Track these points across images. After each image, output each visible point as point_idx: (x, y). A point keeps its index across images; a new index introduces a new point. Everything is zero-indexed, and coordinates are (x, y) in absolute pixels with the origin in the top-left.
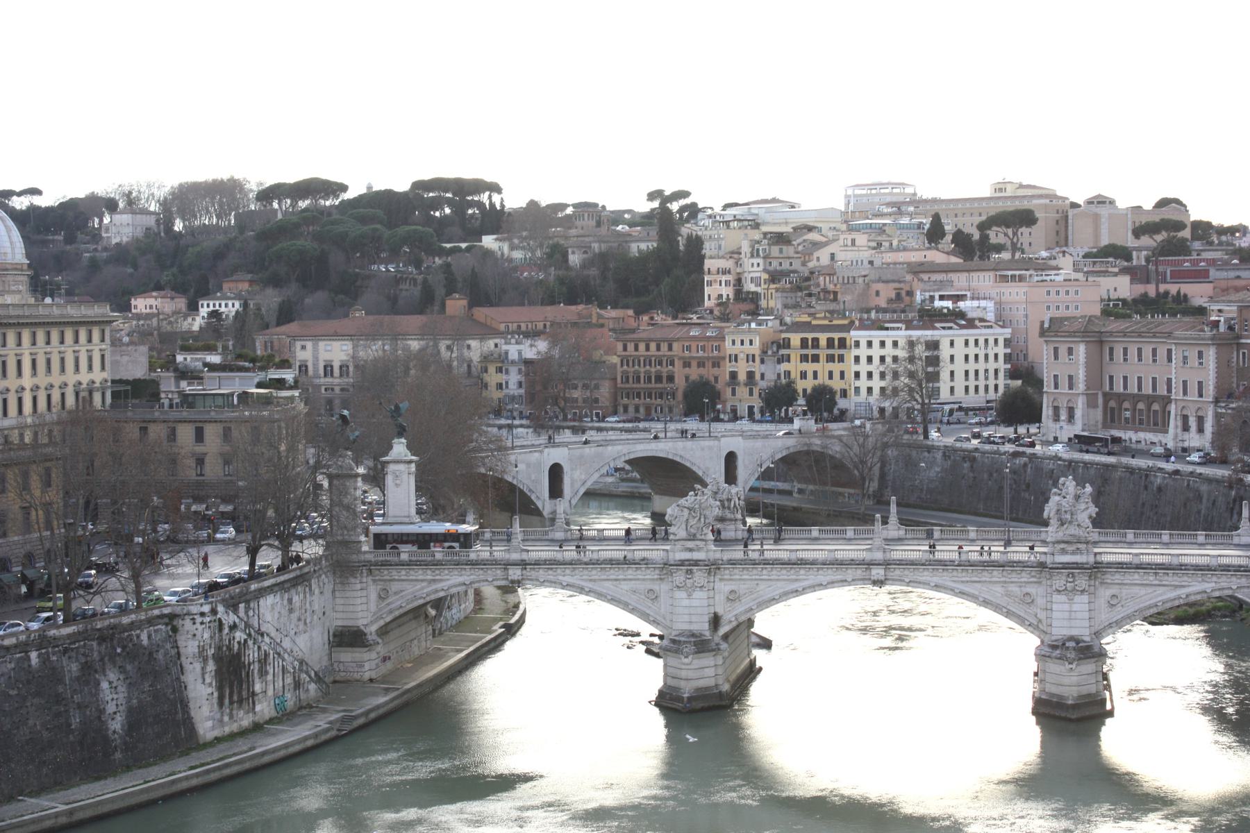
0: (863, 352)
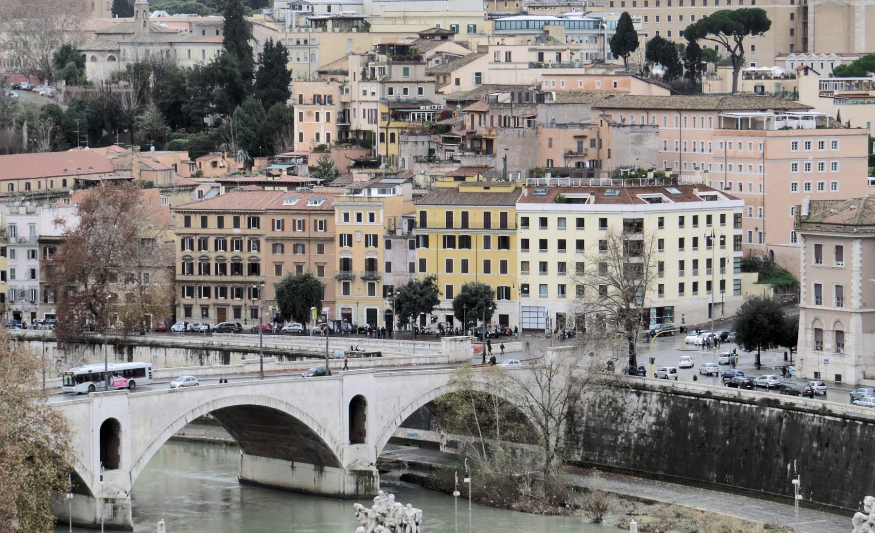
0: (534, 234)
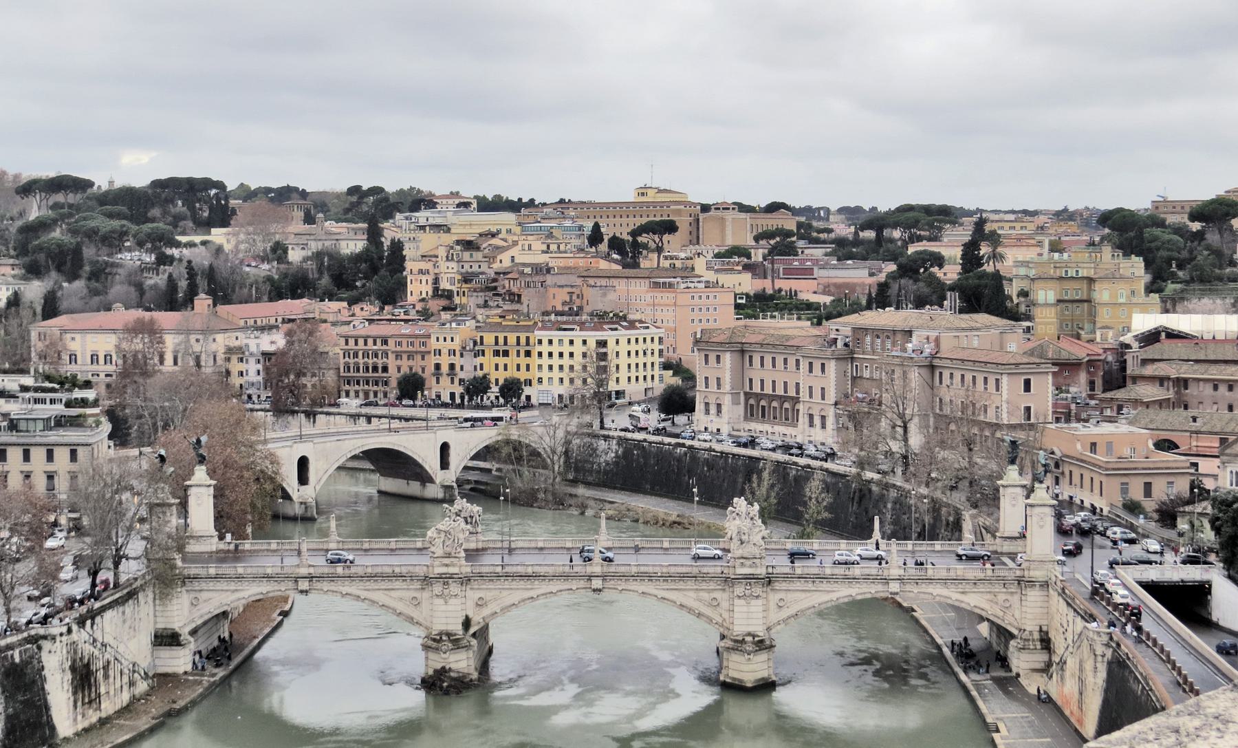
0: (545, 348)
